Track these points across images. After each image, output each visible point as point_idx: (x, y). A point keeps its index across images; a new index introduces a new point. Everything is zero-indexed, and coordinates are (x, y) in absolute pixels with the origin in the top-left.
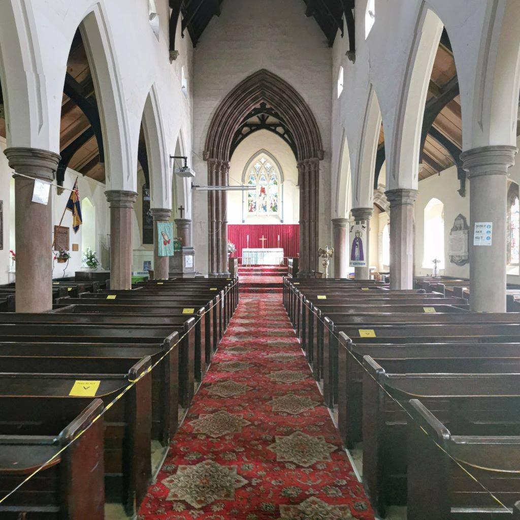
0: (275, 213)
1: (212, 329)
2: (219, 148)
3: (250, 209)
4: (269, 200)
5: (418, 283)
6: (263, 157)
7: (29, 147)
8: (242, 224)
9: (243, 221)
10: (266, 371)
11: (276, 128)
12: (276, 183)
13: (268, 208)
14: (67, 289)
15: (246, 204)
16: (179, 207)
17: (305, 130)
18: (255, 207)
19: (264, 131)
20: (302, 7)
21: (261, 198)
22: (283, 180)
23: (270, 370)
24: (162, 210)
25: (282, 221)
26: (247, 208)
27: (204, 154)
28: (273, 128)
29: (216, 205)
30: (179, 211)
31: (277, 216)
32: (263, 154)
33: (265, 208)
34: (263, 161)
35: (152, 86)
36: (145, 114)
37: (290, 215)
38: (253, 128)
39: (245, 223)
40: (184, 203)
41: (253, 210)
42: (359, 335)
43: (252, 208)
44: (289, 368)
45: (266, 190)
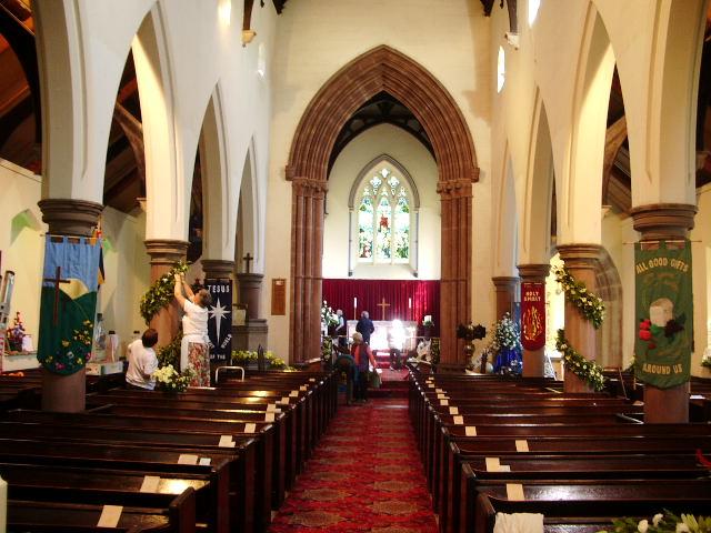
0: (405, 261)
1: (303, 438)
2: (315, 158)
3: (362, 252)
4: (398, 240)
5: (478, 493)
6: (384, 168)
7: (68, 198)
8: (347, 277)
9: (350, 274)
10: (367, 501)
11: (406, 122)
12: (406, 210)
13: (393, 252)
14: (243, 426)
15: (355, 245)
16: (245, 255)
17: (432, 447)
18: (370, 250)
19: (385, 127)
20: (465, 10)
21: (381, 235)
22: (417, 206)
23: (373, 499)
24: (221, 263)
25: (416, 275)
26: (356, 252)
27: (287, 170)
28: (402, 121)
29: (306, 245)
30: (244, 262)
31: (407, 266)
32: (385, 163)
33: (386, 251)
34: (385, 173)
35: (217, 86)
36: (205, 132)
37: (429, 266)
38: (369, 121)
39: (354, 277)
40: (252, 250)
41: (367, 254)
42: (505, 494)
43: (365, 251)
44: (398, 479)
45: (389, 221)
